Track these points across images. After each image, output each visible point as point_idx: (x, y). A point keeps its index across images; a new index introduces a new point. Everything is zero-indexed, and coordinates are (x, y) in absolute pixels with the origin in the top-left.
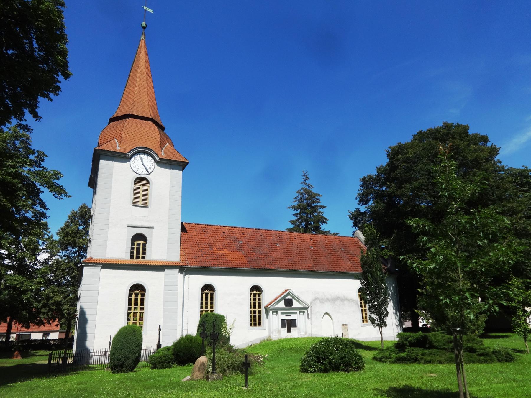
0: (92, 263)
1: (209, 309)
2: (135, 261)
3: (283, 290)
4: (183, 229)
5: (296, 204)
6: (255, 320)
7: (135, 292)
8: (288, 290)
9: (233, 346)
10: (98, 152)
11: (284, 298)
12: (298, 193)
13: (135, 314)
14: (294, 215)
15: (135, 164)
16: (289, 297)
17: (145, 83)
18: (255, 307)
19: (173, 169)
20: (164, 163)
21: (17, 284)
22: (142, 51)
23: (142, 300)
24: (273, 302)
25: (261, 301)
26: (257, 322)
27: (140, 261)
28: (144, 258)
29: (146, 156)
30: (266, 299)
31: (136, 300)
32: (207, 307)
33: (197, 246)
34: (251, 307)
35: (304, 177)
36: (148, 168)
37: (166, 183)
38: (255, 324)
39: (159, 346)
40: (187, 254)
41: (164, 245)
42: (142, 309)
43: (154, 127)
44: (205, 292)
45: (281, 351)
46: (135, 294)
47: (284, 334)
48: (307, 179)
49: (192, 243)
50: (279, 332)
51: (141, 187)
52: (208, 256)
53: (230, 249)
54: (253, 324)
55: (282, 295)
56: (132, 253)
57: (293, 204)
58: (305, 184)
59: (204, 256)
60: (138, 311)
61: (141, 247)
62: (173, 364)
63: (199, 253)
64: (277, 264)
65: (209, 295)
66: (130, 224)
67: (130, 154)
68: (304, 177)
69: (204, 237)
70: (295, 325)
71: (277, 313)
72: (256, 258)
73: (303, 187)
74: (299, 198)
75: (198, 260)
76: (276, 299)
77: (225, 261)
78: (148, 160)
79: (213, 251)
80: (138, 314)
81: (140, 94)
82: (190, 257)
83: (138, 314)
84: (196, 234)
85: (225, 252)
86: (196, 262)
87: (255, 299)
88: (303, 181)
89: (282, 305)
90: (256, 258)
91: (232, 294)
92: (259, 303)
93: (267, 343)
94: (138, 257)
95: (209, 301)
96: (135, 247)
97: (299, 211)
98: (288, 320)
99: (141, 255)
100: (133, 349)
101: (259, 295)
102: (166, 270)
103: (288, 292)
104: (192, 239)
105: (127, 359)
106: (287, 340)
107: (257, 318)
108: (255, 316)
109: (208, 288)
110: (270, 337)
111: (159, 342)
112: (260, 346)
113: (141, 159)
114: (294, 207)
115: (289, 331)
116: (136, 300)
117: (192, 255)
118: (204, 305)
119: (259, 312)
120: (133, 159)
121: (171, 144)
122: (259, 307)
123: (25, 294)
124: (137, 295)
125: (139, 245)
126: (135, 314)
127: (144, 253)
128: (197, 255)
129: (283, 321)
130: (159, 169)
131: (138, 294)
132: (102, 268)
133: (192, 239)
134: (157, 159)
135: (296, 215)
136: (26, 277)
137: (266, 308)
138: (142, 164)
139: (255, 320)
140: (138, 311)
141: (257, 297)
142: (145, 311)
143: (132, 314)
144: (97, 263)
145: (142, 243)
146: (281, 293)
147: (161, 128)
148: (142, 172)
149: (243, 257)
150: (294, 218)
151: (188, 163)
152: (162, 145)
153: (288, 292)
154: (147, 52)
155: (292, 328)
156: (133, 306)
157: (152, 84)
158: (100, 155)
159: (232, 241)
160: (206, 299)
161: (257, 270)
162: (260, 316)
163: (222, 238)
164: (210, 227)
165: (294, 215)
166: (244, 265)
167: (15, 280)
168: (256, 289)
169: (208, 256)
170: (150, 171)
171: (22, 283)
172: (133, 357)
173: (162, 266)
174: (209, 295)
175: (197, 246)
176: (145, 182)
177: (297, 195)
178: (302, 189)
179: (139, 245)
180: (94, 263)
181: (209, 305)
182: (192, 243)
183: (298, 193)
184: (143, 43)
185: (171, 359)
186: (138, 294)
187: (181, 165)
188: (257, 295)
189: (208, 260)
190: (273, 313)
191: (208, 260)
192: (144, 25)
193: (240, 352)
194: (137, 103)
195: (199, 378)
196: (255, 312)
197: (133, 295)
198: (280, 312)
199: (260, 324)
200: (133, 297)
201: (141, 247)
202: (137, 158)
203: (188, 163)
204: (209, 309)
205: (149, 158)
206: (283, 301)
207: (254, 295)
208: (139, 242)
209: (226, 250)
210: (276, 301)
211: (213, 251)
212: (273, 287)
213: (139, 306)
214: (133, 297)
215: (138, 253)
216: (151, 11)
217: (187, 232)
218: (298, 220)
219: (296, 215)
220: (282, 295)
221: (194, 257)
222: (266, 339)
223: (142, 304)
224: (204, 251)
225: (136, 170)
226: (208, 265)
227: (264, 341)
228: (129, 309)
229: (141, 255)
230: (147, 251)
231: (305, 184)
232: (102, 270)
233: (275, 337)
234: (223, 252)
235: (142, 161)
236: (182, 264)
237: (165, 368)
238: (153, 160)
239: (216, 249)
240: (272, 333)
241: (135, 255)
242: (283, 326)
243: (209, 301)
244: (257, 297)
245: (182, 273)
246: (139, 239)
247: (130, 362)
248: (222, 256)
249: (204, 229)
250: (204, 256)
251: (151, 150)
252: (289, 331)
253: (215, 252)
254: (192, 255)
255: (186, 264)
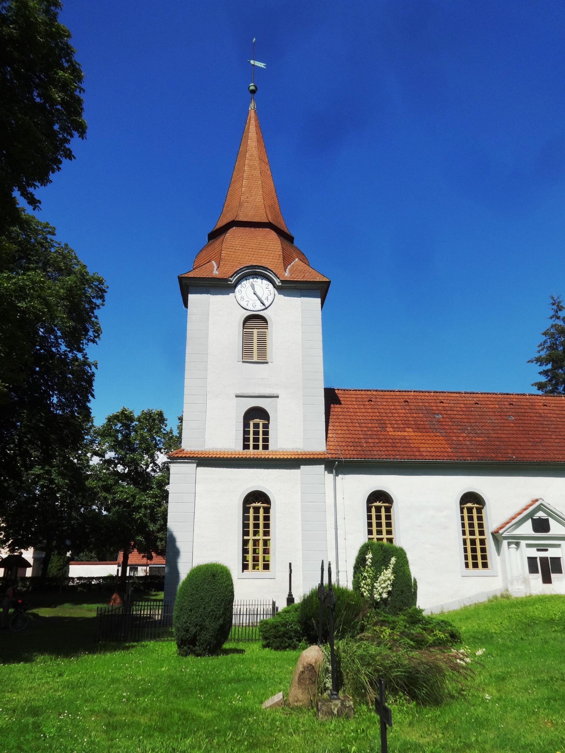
0: (181, 458)
1: (384, 536)
2: (251, 453)
3: (527, 501)
4: (331, 397)
5: (543, 354)
6: (475, 558)
7: (254, 505)
8: (537, 500)
9: (421, 611)
10: (184, 282)
11: (530, 516)
12: (545, 334)
13: (256, 542)
14: (540, 373)
15: (243, 294)
16: (541, 514)
17: (257, 173)
18: (472, 533)
19: (304, 296)
20: (288, 288)
21: (127, 498)
22: (251, 127)
23: (267, 518)
24: (507, 523)
25: (484, 522)
26: (480, 561)
27: (261, 453)
28: (266, 447)
29: (259, 280)
30: (494, 517)
31: (256, 518)
32: (379, 532)
33: (357, 425)
34: (464, 533)
35: (555, 307)
36: (263, 299)
37: (296, 322)
38: (475, 565)
39: (290, 600)
40: (339, 440)
41: (298, 426)
42: (267, 533)
43: (273, 235)
44: (375, 504)
45: (529, 625)
46: (254, 508)
47: (536, 585)
48: (560, 308)
49: (349, 421)
50: (526, 582)
51: (255, 331)
52: (377, 441)
53: (418, 428)
54: (470, 565)
55: (525, 509)
56: (246, 440)
57: (537, 355)
58: (558, 318)
59: (370, 441)
60: (261, 537)
61: (261, 430)
62: (300, 641)
63: (362, 436)
64: (510, 451)
65: (383, 510)
66: (239, 392)
67: (234, 280)
68: (555, 307)
69: (370, 410)
70: (558, 570)
71: (517, 544)
72: (468, 443)
73: (554, 323)
74: (549, 344)
75: (359, 448)
76: (513, 518)
77: (409, 449)
78: (263, 287)
79: (386, 433)
80: (261, 543)
81: (252, 189)
82: (344, 444)
83: (261, 543)
84: (356, 406)
85: (409, 433)
86: (354, 452)
87: (471, 518)
88: (552, 313)
89: (527, 528)
90: (468, 443)
91: (426, 506)
92: (481, 526)
93: (500, 604)
94: (256, 447)
95: (384, 521)
96: (252, 429)
97: (549, 366)
98: (544, 560)
99: (261, 443)
100: (212, 611)
101: (479, 511)
102: (302, 467)
103: (537, 504)
104: (349, 414)
105: (201, 630)
106: (542, 599)
107: (479, 554)
108: (474, 550)
109: (379, 500)
110: (507, 590)
111: (290, 595)
112: (486, 608)
113: (253, 286)
114: (539, 360)
115: (547, 580)
116: (256, 518)
117: (349, 440)
118: (374, 528)
119: (482, 542)
120: (239, 288)
121: (304, 259)
122: (482, 533)
123: (138, 512)
124: (257, 510)
125: (256, 426)
126: (256, 542)
127: (266, 440)
128: (357, 440)
129: (532, 561)
130: (282, 299)
131: (259, 508)
132: (199, 465)
133: (349, 414)
134: (277, 282)
135: (545, 373)
136: (140, 489)
137: (495, 535)
138: (254, 293)
139: (475, 558)
140: (261, 537)
141: (475, 514)
142: (271, 537)
143: (251, 543)
144: (189, 458)
145: (261, 422)
146: (523, 506)
147: (286, 237)
148: (255, 307)
149: (444, 442)
150: (543, 379)
151: (329, 283)
152: (287, 261)
153: (537, 504)
154: (261, 127)
155: (553, 576)
156: (251, 529)
157: (269, 172)
158: (188, 286)
159: (421, 415)
160: (379, 517)
161: (470, 463)
162: (483, 550)
163: (404, 411)
164: (381, 393)
165: (540, 373)
166: (446, 454)
167: (126, 492)
168: (472, 501)
169: (377, 441)
170: (267, 304)
171: (134, 496)
172: (213, 626)
173: (295, 460)
174: (383, 510)
175: (357, 425)
176: (262, 324)
177: (544, 338)
178: (552, 326)
179: (256, 426)
180: (185, 458)
181: (384, 528)
182: (349, 421)
183: (545, 334)
184: (252, 114)
185: (296, 632)
186: (259, 508)
187: (319, 289)
188: (475, 511)
189: (377, 449)
190: (509, 544)
191: (377, 449)
192: (252, 88)
193: (438, 624)
194: (245, 204)
195: (299, 704)
196: (473, 542)
197: (251, 510)
198: (523, 543)
199: (485, 565)
200: (251, 514)
201: (261, 430)
202: (246, 284)
203: (329, 283)
204: (384, 536)
205: (265, 282)
206: (529, 523)
207: (470, 510)
208: (257, 421)
209: (410, 430)
210: (514, 522)
211: (386, 433)
212: (506, 495)
213: (261, 529)
214: (251, 514)
215: (256, 440)
216: (261, 65)
217: (340, 404)
218: (550, 381)
219: (545, 373)
220: (525, 509)
221: (351, 444)
222: (499, 595)
223: (267, 526)
224: (370, 433)
225: (244, 304)
226: (377, 457)
227: (495, 597)
228: (246, 533)
229: (261, 443)
230: (271, 436)
231: (558, 318)
232: (200, 469)
233: (519, 591)
234: (406, 434)
235: (253, 289)
236: (329, 456)
237: (285, 648)
238: (271, 286)
239: (391, 429)
240: (512, 583)
241: (251, 443)
242: (533, 568)
243: (384, 521)
244: (475, 514)
245: (330, 472)
246: (256, 418)
247: (206, 636)
248: (404, 441)
249: (370, 398)
250: (370, 441)
251: (266, 269)
252: (547, 580)
253: (390, 433)
254: (349, 440)
255: (337, 456)
